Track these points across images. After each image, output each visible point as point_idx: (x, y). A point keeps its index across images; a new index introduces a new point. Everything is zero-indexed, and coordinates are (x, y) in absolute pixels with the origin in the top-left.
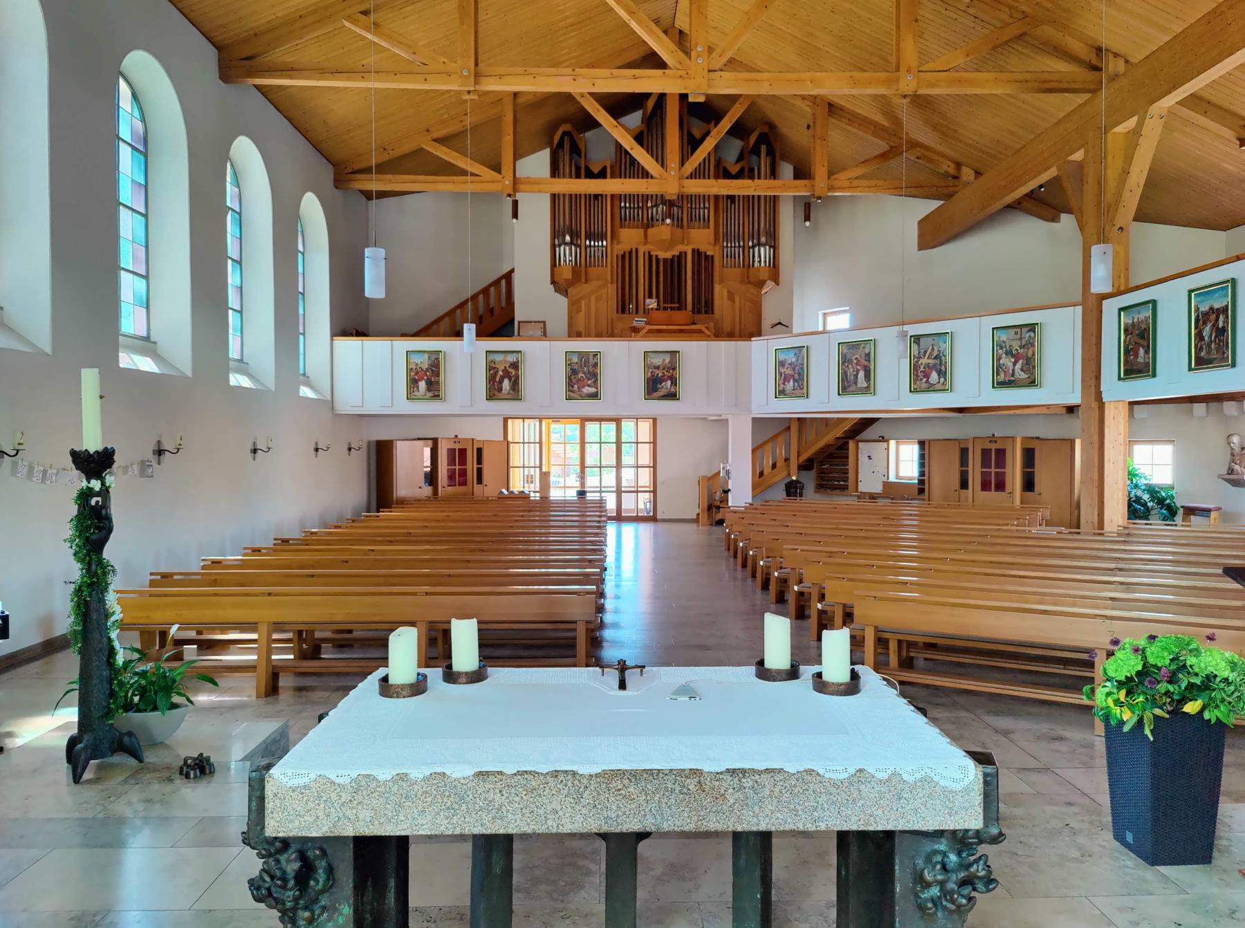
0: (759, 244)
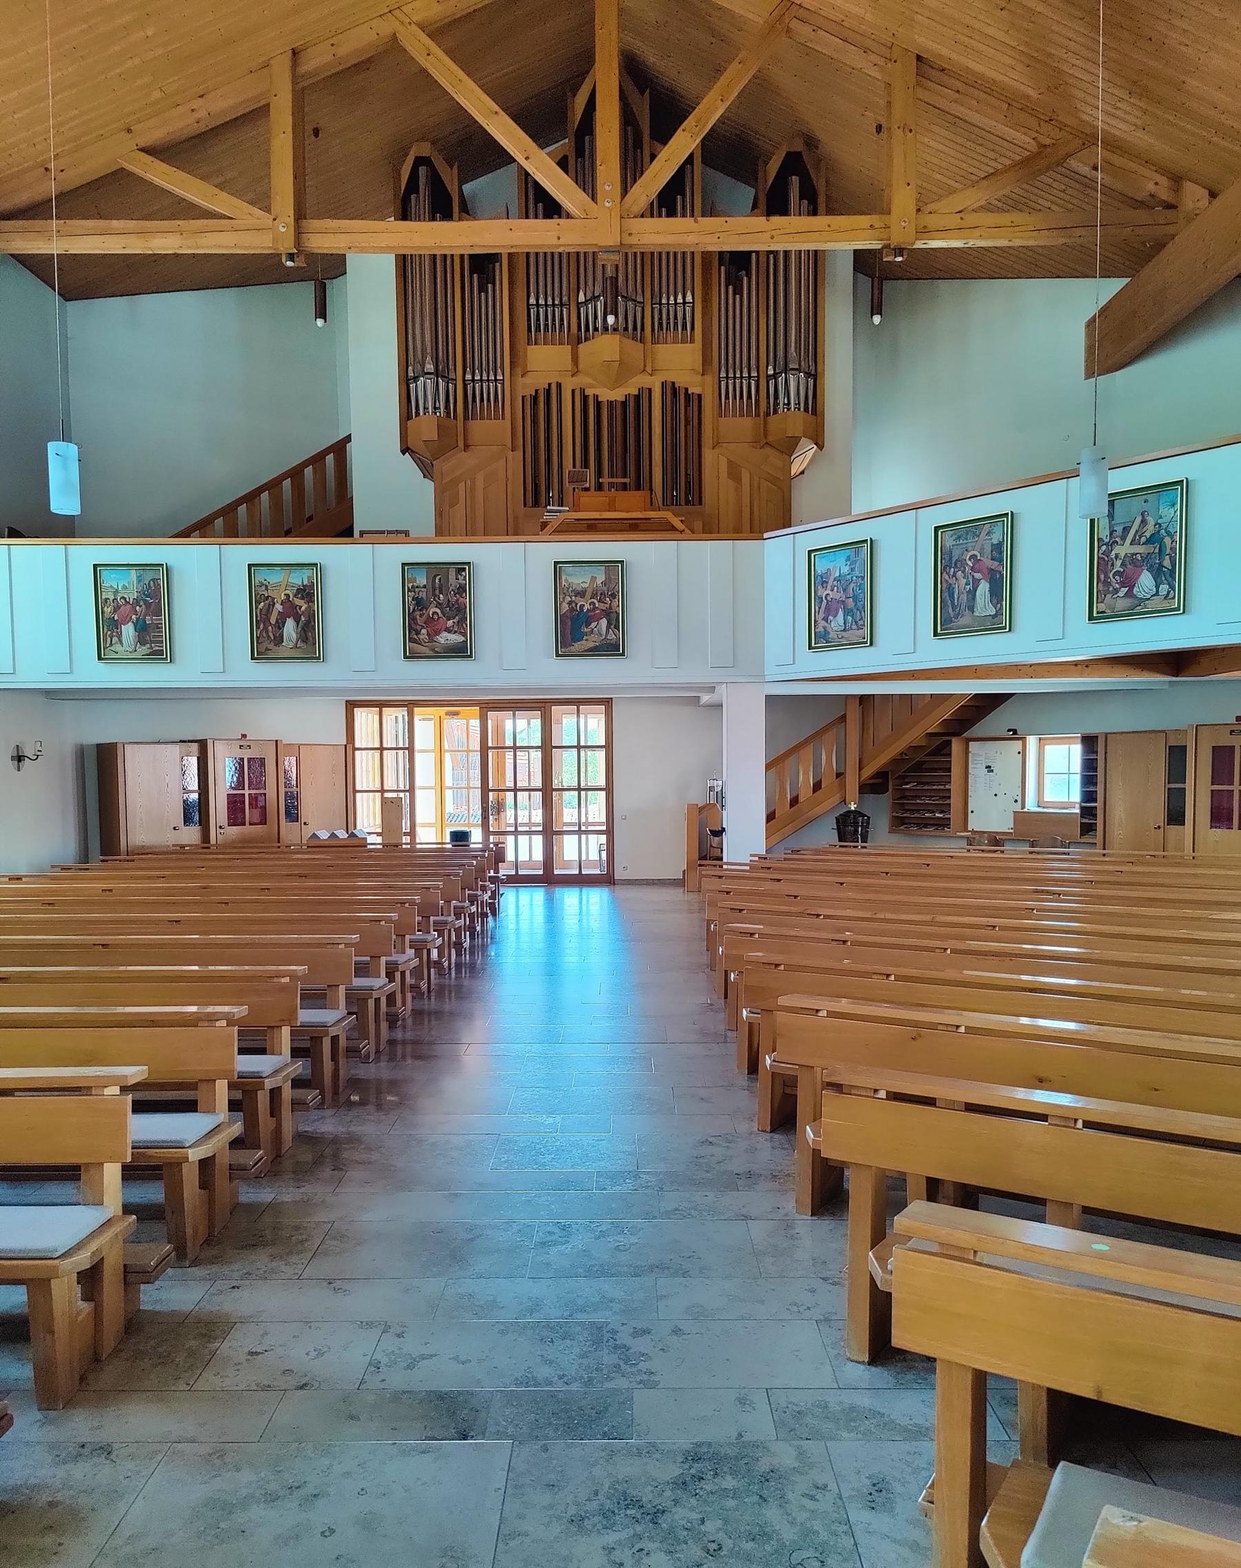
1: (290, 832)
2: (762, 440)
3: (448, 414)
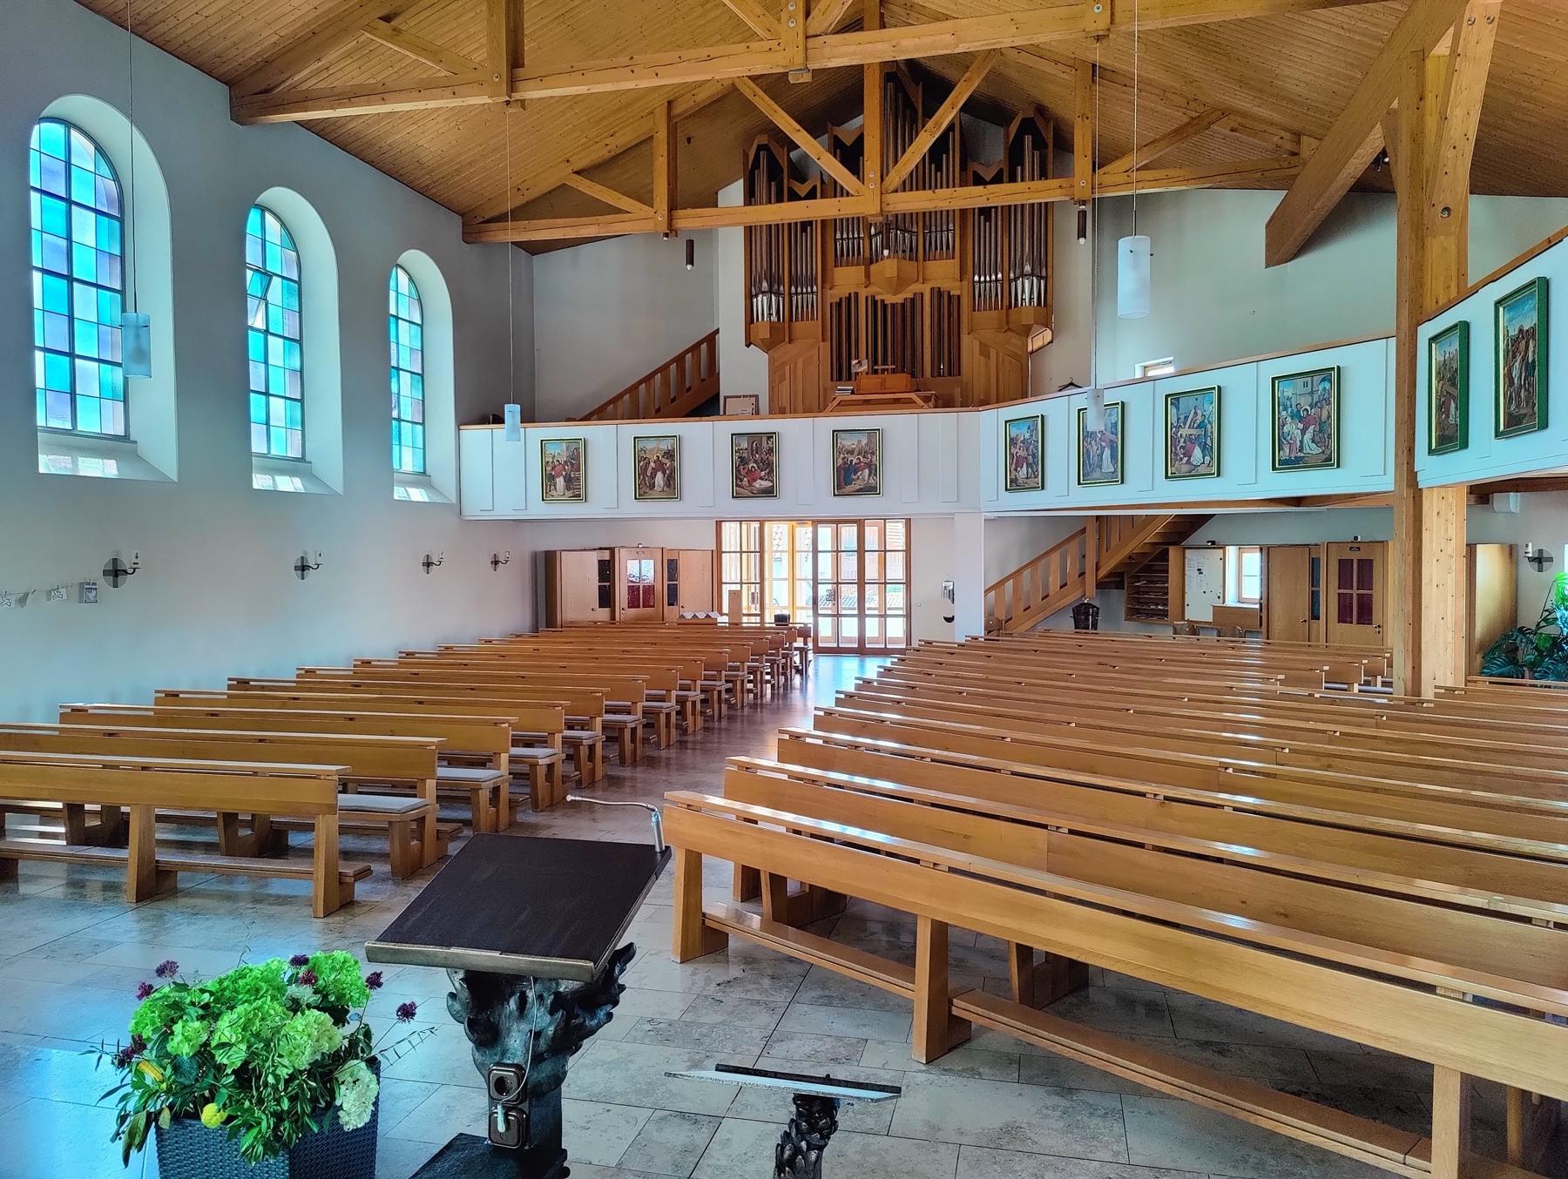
0: (1023, 275)
1: (671, 613)
2: (1007, 326)
3: (779, 318)
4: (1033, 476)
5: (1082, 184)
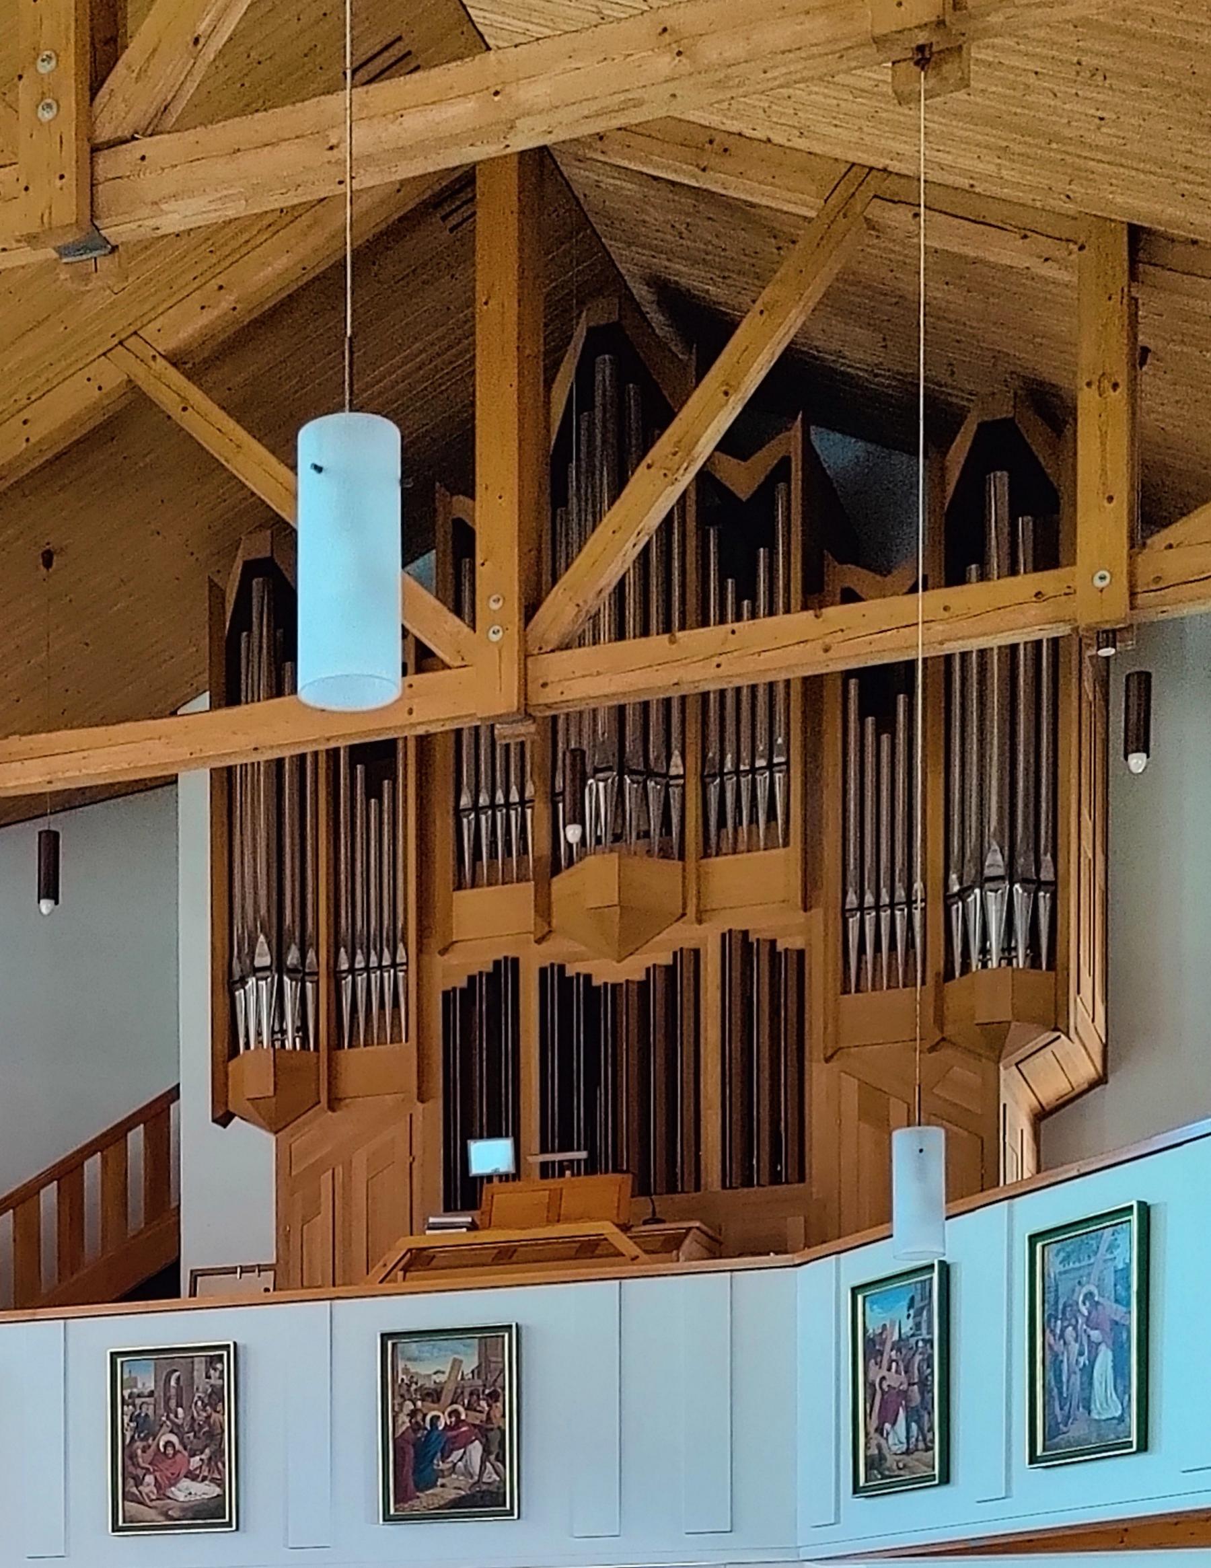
0: (983, 881)
3: (305, 1040)
4: (921, 1445)
5: (1099, 584)
